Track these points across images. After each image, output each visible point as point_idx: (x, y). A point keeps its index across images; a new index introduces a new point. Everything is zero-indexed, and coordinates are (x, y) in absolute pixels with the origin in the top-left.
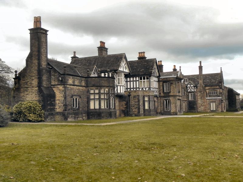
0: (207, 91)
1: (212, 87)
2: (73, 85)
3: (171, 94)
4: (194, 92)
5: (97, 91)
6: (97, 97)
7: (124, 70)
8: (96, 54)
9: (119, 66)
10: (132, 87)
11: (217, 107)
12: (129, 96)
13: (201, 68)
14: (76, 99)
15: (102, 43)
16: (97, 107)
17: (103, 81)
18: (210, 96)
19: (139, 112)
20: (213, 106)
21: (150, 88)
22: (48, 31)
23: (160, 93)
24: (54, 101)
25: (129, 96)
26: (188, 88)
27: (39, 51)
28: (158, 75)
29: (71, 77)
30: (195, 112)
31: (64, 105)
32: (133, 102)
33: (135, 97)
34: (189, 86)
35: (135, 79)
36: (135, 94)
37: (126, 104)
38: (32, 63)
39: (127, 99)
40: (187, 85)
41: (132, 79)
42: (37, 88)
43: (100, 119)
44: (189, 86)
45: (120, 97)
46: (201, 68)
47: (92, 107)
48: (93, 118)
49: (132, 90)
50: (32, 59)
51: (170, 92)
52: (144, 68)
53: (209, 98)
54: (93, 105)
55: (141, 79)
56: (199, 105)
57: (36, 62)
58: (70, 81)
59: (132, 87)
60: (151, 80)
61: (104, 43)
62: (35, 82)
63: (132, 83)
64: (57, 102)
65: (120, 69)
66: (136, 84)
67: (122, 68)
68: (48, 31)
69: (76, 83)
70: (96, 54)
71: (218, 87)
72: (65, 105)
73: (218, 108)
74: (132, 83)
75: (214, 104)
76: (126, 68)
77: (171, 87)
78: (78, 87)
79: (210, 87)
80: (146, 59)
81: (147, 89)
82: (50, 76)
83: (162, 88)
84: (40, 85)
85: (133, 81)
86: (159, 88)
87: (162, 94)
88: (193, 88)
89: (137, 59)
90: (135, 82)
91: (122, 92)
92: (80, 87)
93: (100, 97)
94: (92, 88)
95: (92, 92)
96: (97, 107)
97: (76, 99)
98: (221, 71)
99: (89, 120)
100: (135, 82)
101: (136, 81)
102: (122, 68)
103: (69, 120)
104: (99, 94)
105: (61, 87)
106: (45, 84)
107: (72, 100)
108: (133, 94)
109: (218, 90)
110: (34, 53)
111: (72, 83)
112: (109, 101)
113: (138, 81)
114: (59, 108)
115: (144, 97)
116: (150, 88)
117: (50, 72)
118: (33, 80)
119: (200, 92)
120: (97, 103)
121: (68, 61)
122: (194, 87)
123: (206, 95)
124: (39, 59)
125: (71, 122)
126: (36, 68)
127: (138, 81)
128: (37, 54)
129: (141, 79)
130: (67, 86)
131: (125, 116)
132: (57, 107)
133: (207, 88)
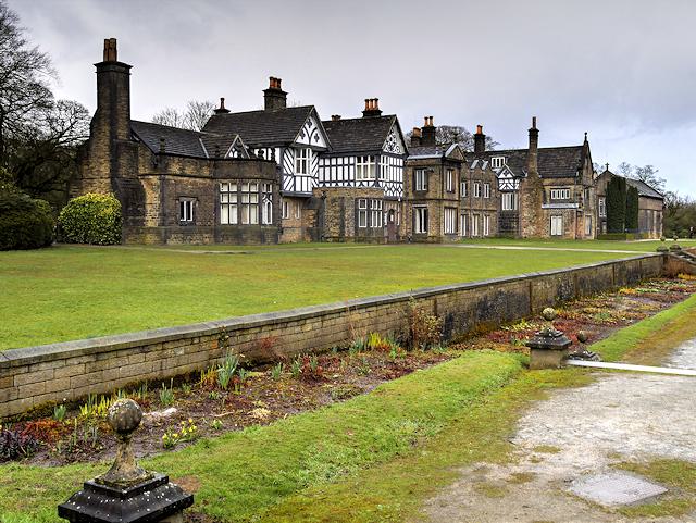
0: (547, 188)
1: (559, 181)
2: (181, 176)
3: (430, 195)
4: (512, 191)
5: (234, 189)
6: (234, 200)
7: (313, 142)
8: (259, 104)
9: (298, 132)
10: (340, 178)
11: (566, 226)
12: (323, 198)
13: (534, 134)
14: (188, 204)
15: (275, 81)
16: (234, 221)
17: (247, 168)
18: (552, 202)
19: (342, 232)
20: (557, 226)
21: (376, 183)
22: (131, 67)
23: (407, 194)
24: (144, 206)
25: (323, 198)
26: (501, 182)
27: (112, 108)
28: (402, 152)
29: (176, 159)
30: (513, 239)
31: (159, 215)
32: (329, 213)
33: (334, 200)
34: (502, 176)
35: (327, 163)
36: (335, 195)
37: (317, 216)
38: (100, 131)
39: (317, 206)
40: (499, 174)
41: (334, 162)
42: (109, 181)
43: (239, 244)
44: (502, 176)
45: (302, 200)
46: (534, 134)
47: (224, 220)
48: (226, 242)
49: (328, 185)
50: (99, 124)
51: (428, 191)
52: (365, 133)
53: (548, 206)
54: (227, 217)
55: (359, 161)
56: (523, 223)
57: (106, 129)
58: (175, 168)
59: (340, 178)
60: (381, 164)
61: (279, 81)
62: (105, 169)
63: (334, 169)
64: (149, 208)
65: (299, 140)
66: (349, 173)
67: (306, 138)
68: (131, 67)
69: (188, 171)
70: (259, 104)
71: (571, 180)
72: (163, 215)
73: (567, 230)
74: (340, 169)
75: (560, 221)
76: (317, 138)
77: (431, 180)
78: (192, 180)
79: (553, 180)
80: (382, 114)
81: (371, 184)
82: (136, 156)
83: (411, 182)
84: (114, 174)
85: (343, 165)
86: (405, 181)
87: (411, 196)
88: (512, 181)
89: (361, 116)
90: (346, 168)
91: (304, 189)
92: (197, 180)
93: (239, 200)
94: (225, 181)
95: (225, 189)
96: (234, 221)
97: (188, 204)
98: (586, 142)
99: (83, 254)
100: (327, 169)
101: (349, 165)
102: (306, 138)
103: (170, 242)
104: (239, 194)
105: (155, 179)
106: (123, 172)
107: (179, 206)
108: (331, 195)
109: (572, 187)
110: (104, 111)
111: (178, 172)
112: (260, 210)
113: (353, 165)
114: (151, 221)
115: (356, 199)
116: (376, 183)
117: (135, 149)
118: (101, 164)
119: (530, 190)
120: (234, 212)
121: (331, 119)
122: (514, 179)
123: (541, 200)
124: (113, 124)
125: (174, 247)
126: (107, 142)
127: (353, 165)
128: (108, 112)
129: (359, 161)
130: (167, 177)
131: (313, 241)
132: (148, 218)
133: (547, 182)
